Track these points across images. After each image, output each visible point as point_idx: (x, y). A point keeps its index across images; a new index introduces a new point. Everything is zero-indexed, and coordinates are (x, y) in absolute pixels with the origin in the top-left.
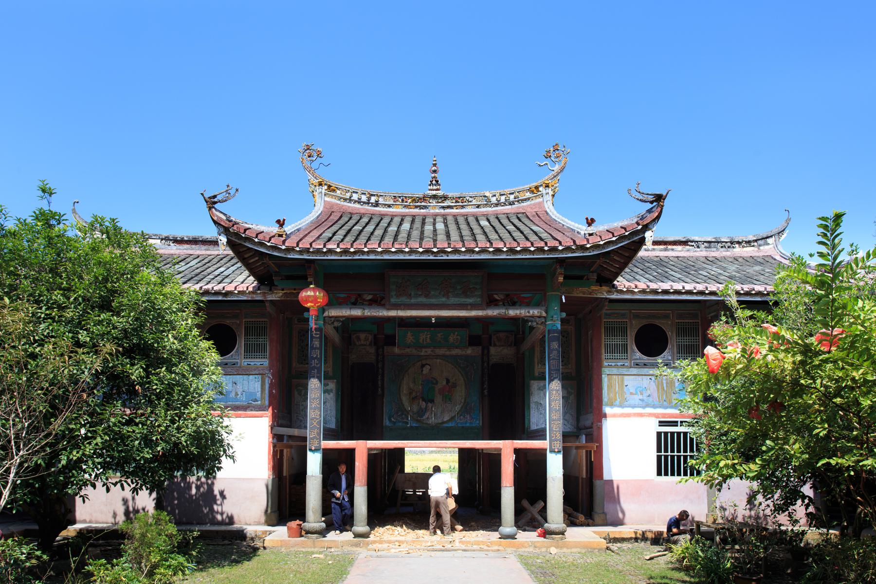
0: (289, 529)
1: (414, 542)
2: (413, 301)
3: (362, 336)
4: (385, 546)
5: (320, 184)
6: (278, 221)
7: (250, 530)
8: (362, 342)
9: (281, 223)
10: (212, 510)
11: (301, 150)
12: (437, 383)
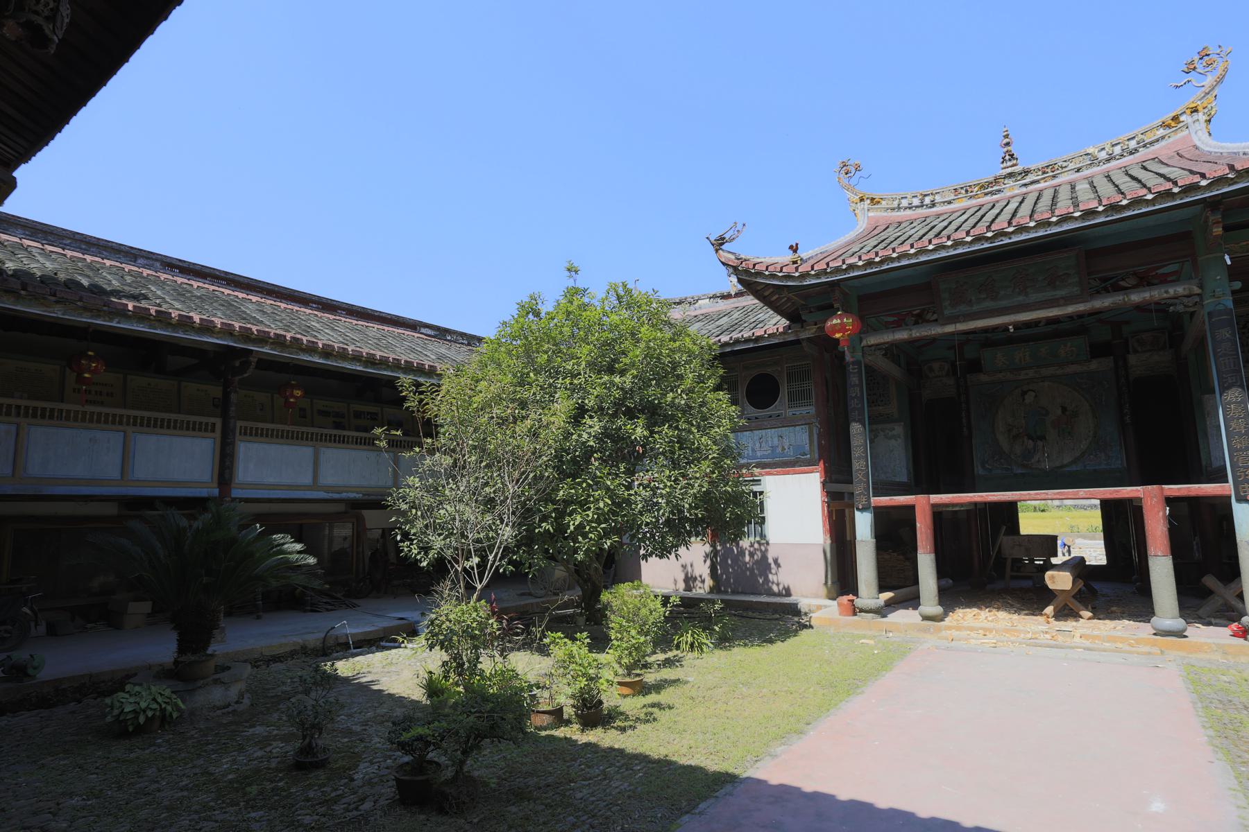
0: (839, 605)
1: (1007, 631)
2: (975, 308)
3: (936, 366)
4: (964, 633)
5: (862, 200)
6: (791, 247)
7: (804, 603)
9: (794, 249)
10: (767, 580)
11: (837, 169)
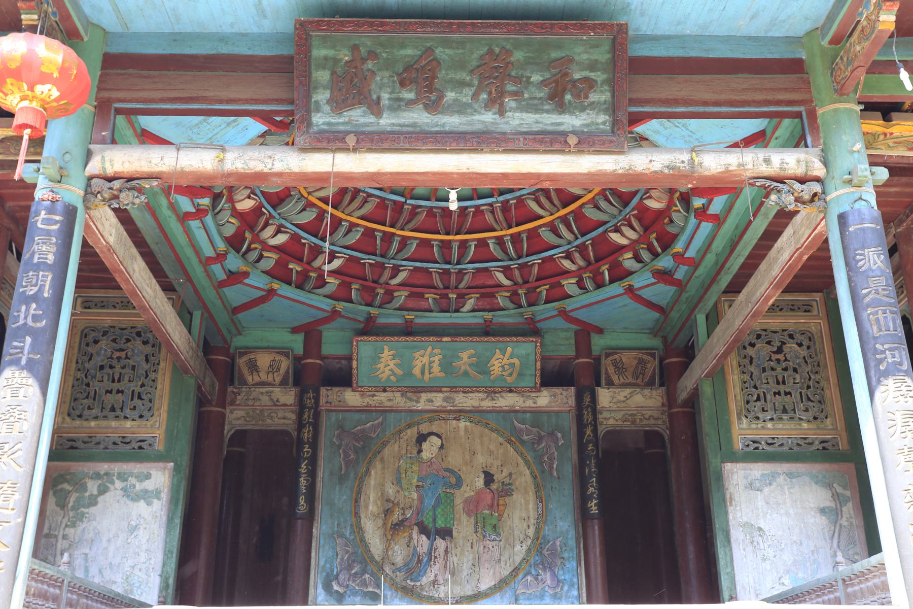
2: (387, 121)
3: (264, 360)
8: (264, 377)
12: (459, 483)
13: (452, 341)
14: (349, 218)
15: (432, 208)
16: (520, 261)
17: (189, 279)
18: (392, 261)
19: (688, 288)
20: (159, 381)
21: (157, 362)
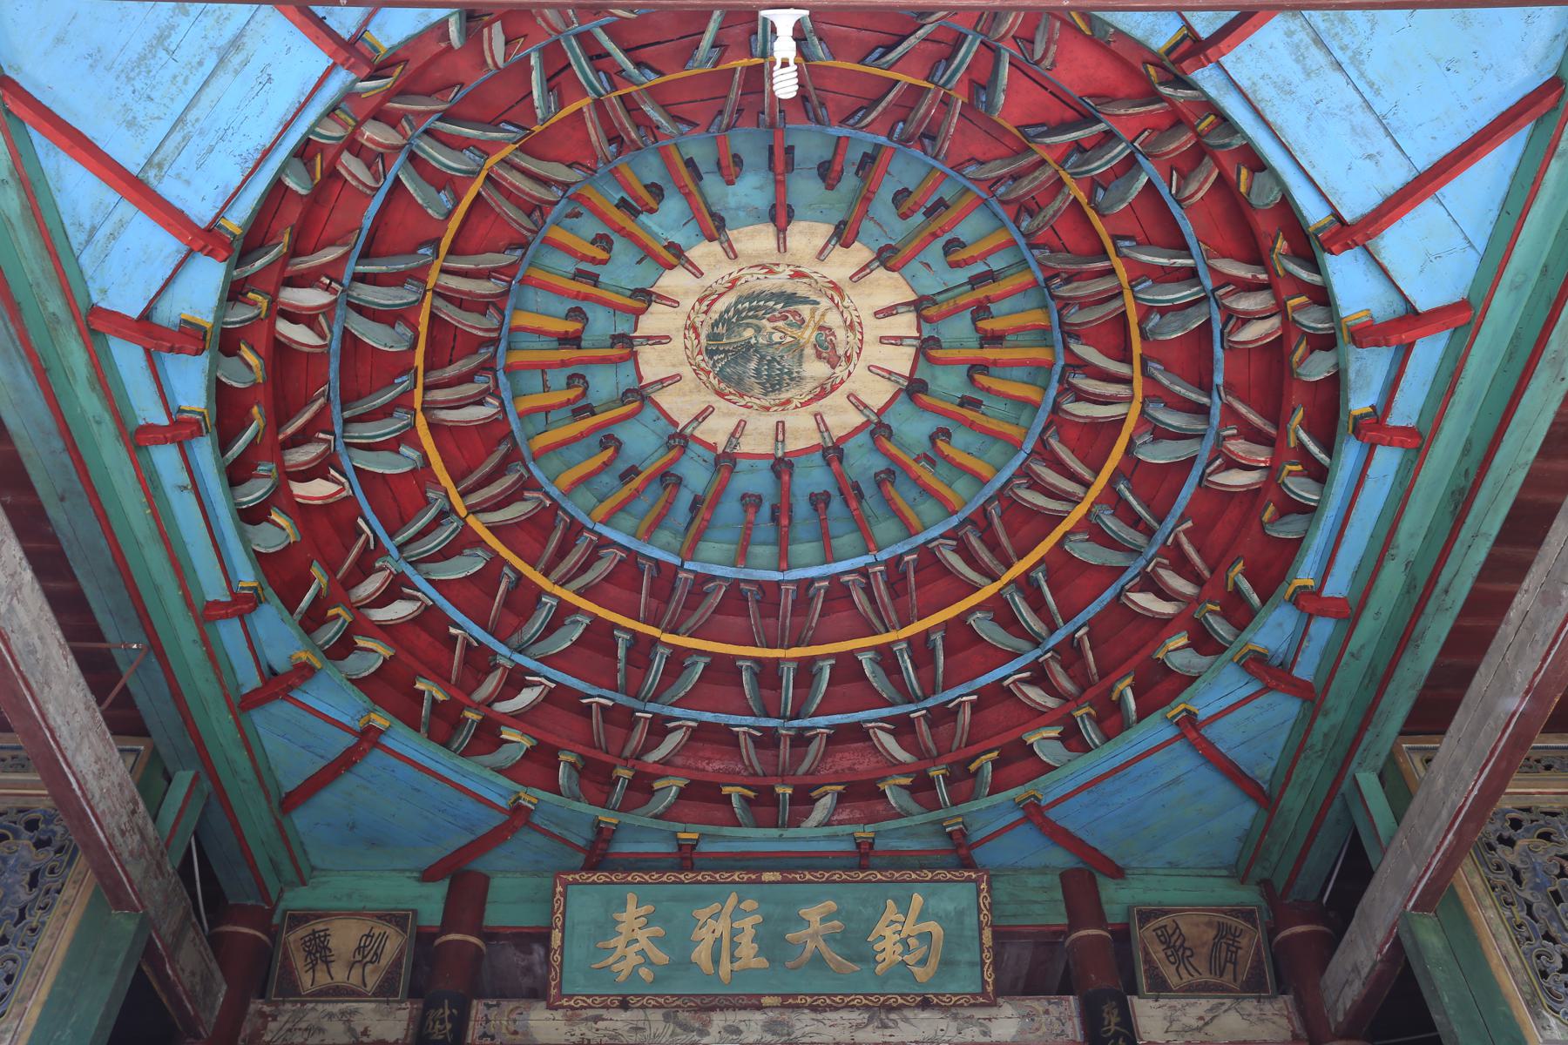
3: (344, 936)
8: (339, 974)
13: (784, 882)
14: (557, 590)
15: (737, 581)
16: (930, 702)
17: (155, 645)
18: (652, 707)
19: (1331, 701)
20: (47, 932)
21: (55, 886)
